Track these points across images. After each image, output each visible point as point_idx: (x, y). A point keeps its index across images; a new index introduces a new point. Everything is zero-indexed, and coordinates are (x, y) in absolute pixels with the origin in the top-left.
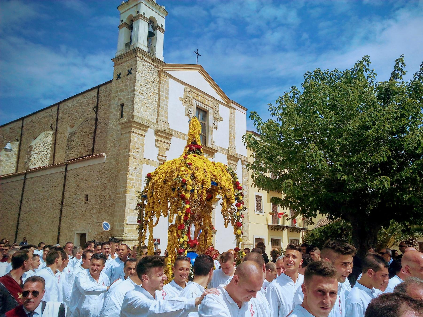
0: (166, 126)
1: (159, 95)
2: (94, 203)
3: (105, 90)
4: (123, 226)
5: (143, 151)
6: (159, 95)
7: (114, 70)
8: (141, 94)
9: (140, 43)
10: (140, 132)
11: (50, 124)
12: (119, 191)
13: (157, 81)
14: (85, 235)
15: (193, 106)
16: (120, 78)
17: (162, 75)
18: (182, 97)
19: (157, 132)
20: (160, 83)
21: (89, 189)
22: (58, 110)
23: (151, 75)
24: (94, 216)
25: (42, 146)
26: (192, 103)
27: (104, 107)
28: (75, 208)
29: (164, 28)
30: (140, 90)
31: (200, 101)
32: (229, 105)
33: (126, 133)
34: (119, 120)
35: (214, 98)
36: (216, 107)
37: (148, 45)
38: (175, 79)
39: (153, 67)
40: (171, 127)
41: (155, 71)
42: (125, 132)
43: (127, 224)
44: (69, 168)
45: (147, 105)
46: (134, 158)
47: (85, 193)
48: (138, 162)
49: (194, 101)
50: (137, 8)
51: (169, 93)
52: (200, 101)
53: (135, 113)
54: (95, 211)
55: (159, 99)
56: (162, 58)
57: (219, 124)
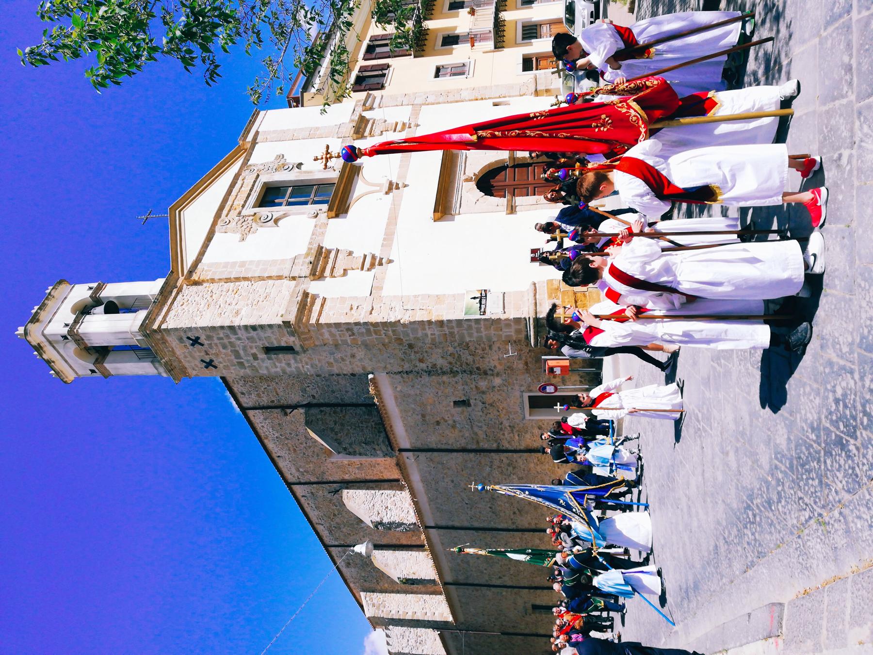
0: (300, 261)
1: (237, 279)
4: (507, 320)
5: (356, 298)
6: (237, 279)
8: (237, 313)
9: (131, 326)
11: (329, 496)
13: (209, 287)
14: (531, 398)
15: (255, 214)
16: (212, 361)
17: (195, 277)
18: (238, 236)
19: (317, 274)
20: (213, 281)
22: (300, 483)
23: (197, 299)
25: (372, 504)
26: (249, 216)
29: (94, 285)
30: (231, 316)
31: (246, 202)
32: (248, 146)
35: (236, 177)
36: (256, 170)
37: (135, 311)
38: (202, 253)
39: (180, 297)
40: (304, 251)
41: (189, 292)
43: (505, 313)
44: (405, 443)
45: (261, 300)
46: (371, 313)
48: (379, 306)
49: (244, 213)
50: (57, 342)
52: (246, 202)
53: (278, 321)
55: (246, 279)
56: (160, 282)
57: (292, 160)
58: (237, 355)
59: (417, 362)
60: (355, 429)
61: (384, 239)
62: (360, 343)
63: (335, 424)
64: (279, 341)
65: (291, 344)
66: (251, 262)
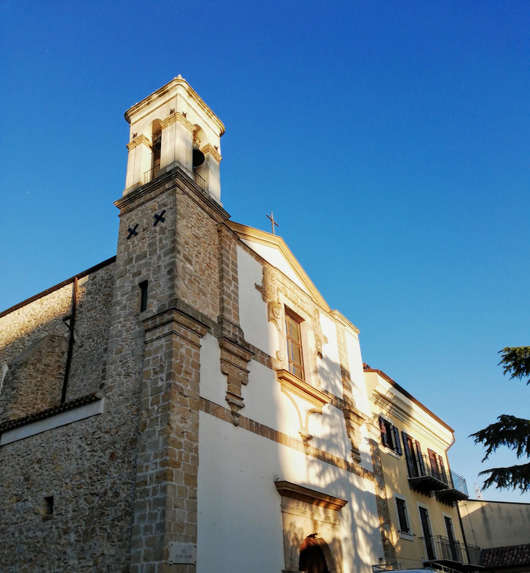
2: (70, 515)
3: (91, 281)
7: (121, 221)
10: (190, 335)
12: (145, 476)
16: (136, 234)
21: (57, 482)
24: (69, 550)
27: (88, 315)
28: (17, 535)
33: (159, 338)
34: (138, 315)
42: (155, 337)
47: (45, 494)
51: (239, 270)
54: (72, 537)
55: (221, 278)
58: (143, 256)
59: (111, 451)
60: (36, 385)
61: (257, 424)
62: (144, 381)
63: (45, 365)
64: (154, 297)
65: (148, 309)
66: (237, 287)
